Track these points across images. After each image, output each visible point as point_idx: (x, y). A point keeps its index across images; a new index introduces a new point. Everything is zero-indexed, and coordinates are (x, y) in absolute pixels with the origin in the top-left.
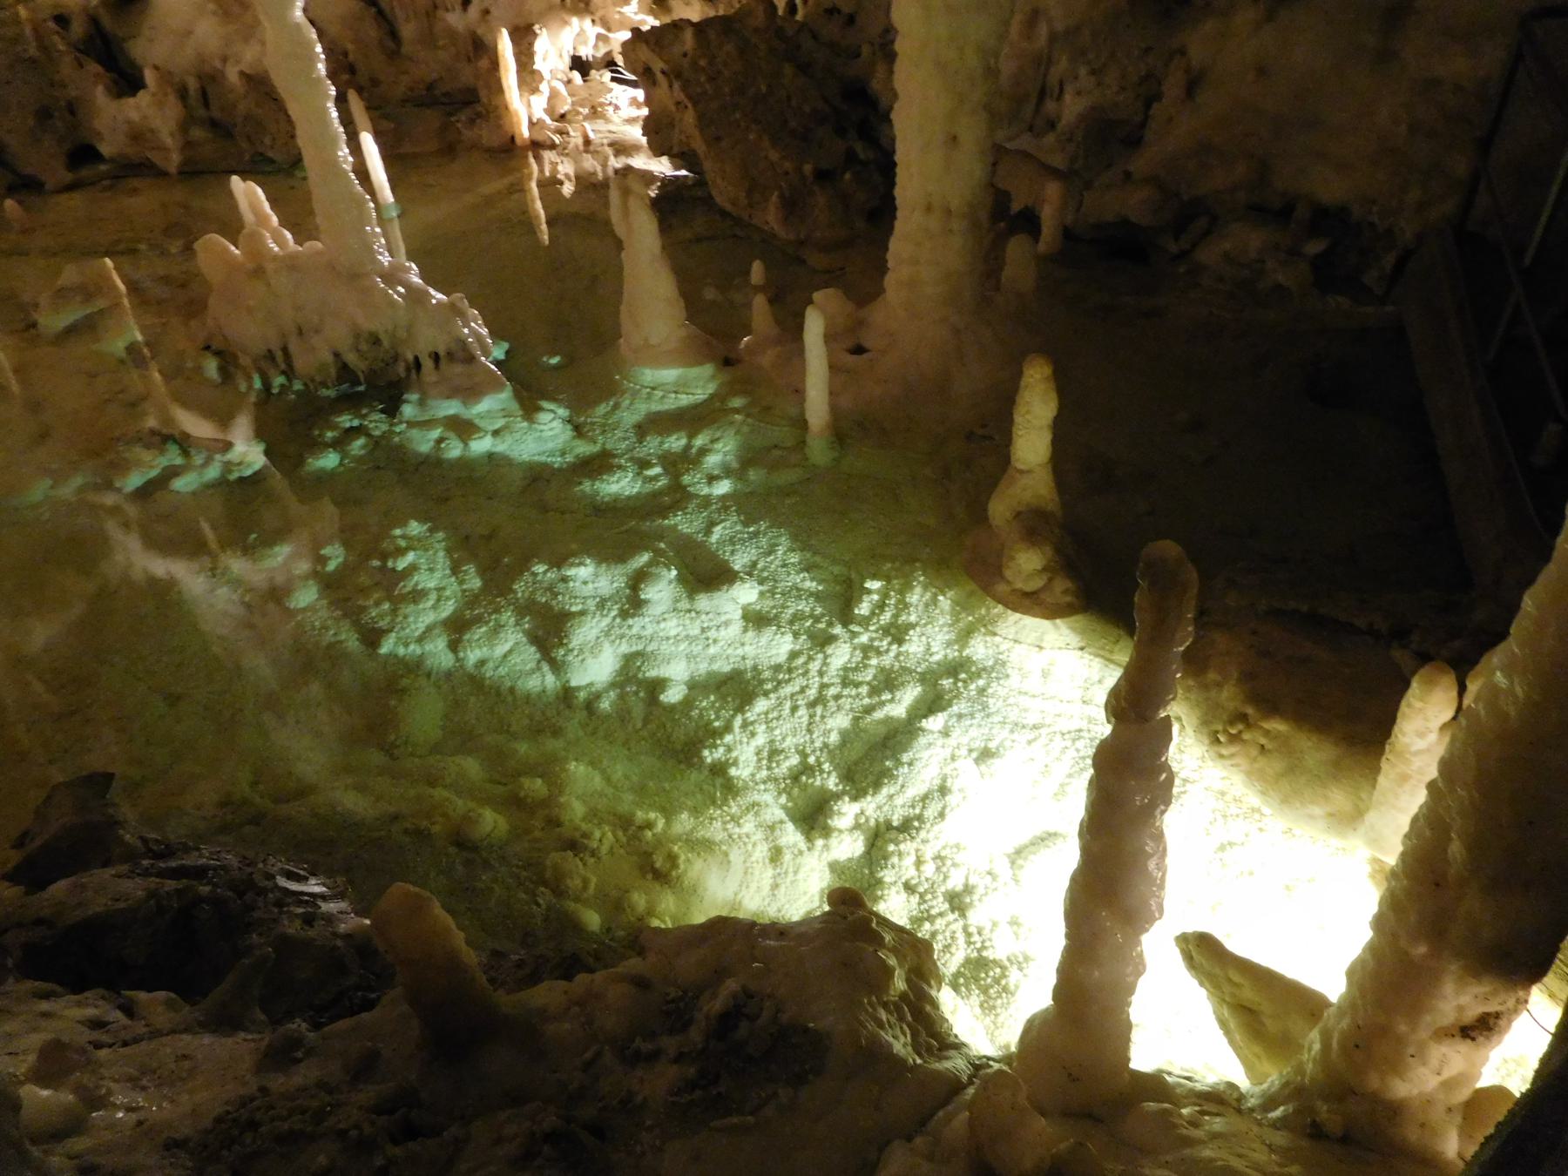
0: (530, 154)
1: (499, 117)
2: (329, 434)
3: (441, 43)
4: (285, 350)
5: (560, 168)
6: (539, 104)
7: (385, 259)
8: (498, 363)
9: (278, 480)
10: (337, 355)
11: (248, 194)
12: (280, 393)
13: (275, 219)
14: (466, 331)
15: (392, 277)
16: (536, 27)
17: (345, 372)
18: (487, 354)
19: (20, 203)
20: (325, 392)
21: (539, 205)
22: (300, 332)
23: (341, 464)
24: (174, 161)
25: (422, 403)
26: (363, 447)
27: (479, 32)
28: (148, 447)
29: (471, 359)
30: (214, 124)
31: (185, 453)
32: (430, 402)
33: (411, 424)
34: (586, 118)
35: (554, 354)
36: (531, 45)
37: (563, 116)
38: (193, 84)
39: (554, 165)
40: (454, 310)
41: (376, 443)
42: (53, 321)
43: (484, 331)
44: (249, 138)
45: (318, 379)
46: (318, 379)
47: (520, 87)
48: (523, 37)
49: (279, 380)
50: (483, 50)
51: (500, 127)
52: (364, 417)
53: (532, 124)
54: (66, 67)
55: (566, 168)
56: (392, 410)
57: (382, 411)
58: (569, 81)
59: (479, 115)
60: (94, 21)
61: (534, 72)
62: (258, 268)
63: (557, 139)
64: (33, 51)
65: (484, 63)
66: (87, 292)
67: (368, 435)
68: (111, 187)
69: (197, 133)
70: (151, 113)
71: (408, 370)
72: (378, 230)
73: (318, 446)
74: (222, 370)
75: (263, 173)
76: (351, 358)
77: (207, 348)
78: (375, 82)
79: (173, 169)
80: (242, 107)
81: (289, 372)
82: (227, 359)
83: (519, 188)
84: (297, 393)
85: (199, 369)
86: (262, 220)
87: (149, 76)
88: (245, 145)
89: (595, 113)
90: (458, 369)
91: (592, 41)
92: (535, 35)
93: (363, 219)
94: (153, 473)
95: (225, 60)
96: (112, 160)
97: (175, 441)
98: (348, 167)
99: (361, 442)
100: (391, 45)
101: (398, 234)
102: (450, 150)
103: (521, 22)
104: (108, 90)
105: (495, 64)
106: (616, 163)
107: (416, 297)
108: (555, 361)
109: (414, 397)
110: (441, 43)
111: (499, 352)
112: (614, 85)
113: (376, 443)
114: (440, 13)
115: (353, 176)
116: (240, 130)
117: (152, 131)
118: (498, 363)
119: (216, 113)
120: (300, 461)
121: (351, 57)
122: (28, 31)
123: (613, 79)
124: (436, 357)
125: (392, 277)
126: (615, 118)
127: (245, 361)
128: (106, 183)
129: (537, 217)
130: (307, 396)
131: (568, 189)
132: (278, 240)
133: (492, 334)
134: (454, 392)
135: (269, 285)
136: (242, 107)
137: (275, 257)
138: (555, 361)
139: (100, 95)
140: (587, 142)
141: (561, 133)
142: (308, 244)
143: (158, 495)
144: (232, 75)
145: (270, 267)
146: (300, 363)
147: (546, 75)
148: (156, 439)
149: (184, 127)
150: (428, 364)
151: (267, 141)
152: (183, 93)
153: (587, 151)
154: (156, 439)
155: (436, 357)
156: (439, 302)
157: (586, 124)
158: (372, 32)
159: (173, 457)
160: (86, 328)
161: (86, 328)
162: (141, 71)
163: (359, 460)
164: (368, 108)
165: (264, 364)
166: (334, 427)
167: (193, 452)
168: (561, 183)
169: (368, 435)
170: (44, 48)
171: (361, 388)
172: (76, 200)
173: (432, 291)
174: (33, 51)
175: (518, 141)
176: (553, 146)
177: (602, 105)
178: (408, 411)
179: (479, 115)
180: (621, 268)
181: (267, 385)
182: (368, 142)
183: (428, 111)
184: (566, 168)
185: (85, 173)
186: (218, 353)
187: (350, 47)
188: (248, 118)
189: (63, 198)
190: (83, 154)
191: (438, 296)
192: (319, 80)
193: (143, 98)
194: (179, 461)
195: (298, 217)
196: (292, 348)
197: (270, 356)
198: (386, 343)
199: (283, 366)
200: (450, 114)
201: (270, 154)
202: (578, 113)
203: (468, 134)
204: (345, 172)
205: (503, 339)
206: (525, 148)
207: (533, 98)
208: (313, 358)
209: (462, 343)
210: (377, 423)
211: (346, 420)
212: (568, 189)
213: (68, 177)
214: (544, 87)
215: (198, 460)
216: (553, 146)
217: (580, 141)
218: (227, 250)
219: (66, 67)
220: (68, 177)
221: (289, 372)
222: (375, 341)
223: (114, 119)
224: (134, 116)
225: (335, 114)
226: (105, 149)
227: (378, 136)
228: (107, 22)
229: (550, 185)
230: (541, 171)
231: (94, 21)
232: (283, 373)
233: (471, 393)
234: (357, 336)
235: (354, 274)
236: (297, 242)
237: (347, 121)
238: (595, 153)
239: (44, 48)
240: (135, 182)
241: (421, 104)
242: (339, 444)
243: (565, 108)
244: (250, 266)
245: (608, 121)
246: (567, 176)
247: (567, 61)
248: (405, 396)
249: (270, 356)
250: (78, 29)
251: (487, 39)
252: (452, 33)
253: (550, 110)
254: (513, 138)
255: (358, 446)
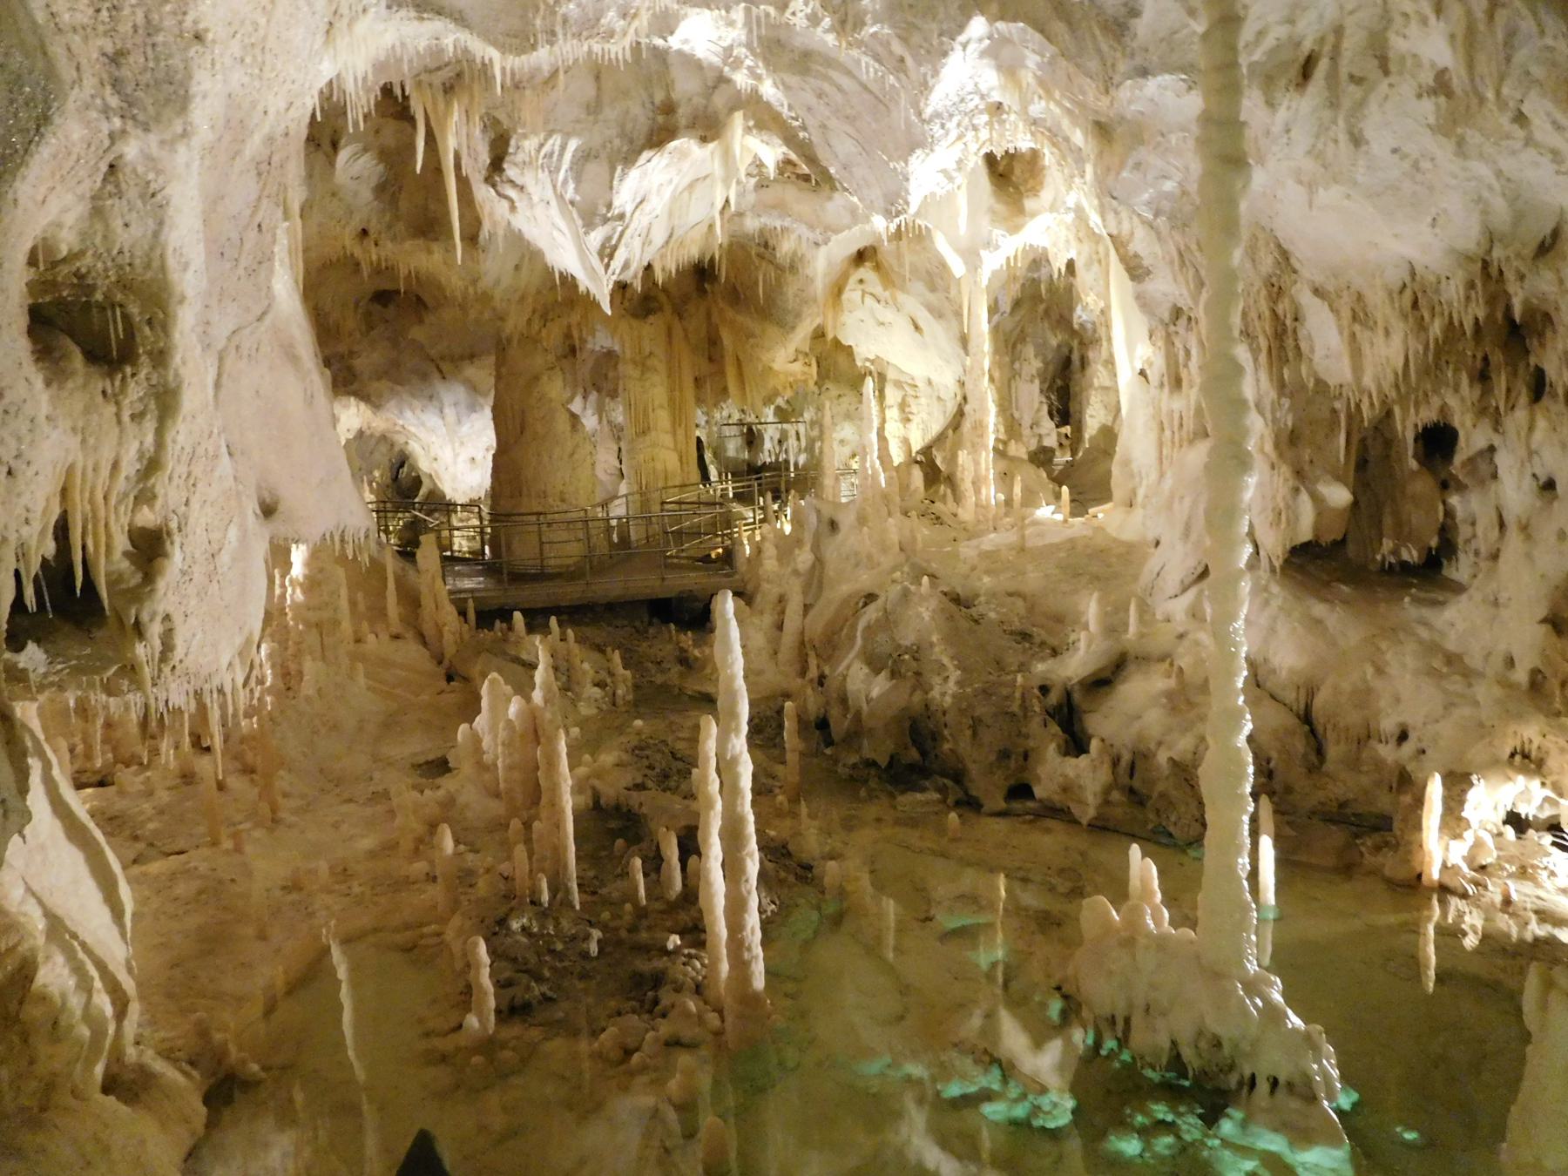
0: (1435, 897)
1: (1410, 852)
2: (1139, 1118)
3: (1365, 768)
4: (1127, 1021)
5: (1467, 918)
6: (1457, 852)
7: (1252, 967)
8: (1340, 1112)
9: (1074, 1146)
10: (1174, 1043)
11: (1142, 867)
12: (1108, 1057)
13: (1159, 896)
14: (1315, 1066)
15: (1252, 987)
16: (1474, 778)
17: (1176, 1062)
18: (1331, 1098)
19: (960, 816)
20: (1149, 1073)
21: (1431, 949)
22: (1147, 1009)
23: (1141, 1156)
24: (1088, 813)
25: (1244, 1125)
26: (1169, 1147)
27: (1409, 768)
28: (976, 1062)
29: (1312, 1099)
30: (1132, 791)
31: (1005, 1079)
32: (1254, 1129)
33: (1226, 1143)
34: (1510, 876)
35: (1410, 1128)
36: (1464, 792)
37: (1483, 868)
38: (1126, 757)
39: (1460, 915)
40: (1307, 1037)
41: (1184, 1148)
42: (949, 921)
43: (1335, 1073)
44: (1158, 811)
45: (1148, 1059)
46: (1148, 1059)
47: (1441, 829)
48: (1457, 783)
49: (1110, 1044)
50: (1407, 785)
51: (1407, 861)
52: (1179, 1115)
53: (1444, 866)
54: (1035, 725)
55: (1473, 920)
56: (1211, 1119)
57: (1200, 1117)
58: (1500, 834)
59: (1387, 844)
60: (1068, 694)
61: (1460, 819)
62: (1130, 939)
63: (1471, 889)
64: (1015, 708)
65: (1407, 799)
66: (972, 900)
67: (1178, 1137)
68: (1031, 822)
69: (1116, 796)
70: (1086, 776)
71: (1241, 1084)
72: (1254, 938)
73: (1122, 1125)
74: (1065, 1014)
75: (1159, 844)
76: (1187, 1053)
77: (1059, 988)
78: (1288, 790)
79: (1085, 822)
80: (1160, 787)
81: (1123, 1042)
82: (1072, 1009)
83: (1415, 929)
84: (1124, 1064)
85: (1044, 1006)
86: (1146, 893)
87: (1094, 745)
88: (1152, 816)
89: (1524, 873)
90: (1295, 1104)
91: (1537, 801)
92: (1472, 785)
93: (1242, 925)
94: (972, 1089)
95: (1160, 744)
96: (1041, 801)
97: (1000, 1065)
98: (1244, 875)
99: (1169, 1140)
100: (1313, 758)
101: (1269, 937)
102: (1347, 869)
103: (1459, 769)
104: (1059, 746)
105: (1419, 802)
106: (1536, 929)
107: (1272, 1015)
108: (1410, 1136)
109: (1238, 1114)
110: (1365, 768)
111: (1346, 1101)
112: (1555, 850)
113: (1184, 1148)
114: (1373, 743)
115: (1245, 883)
116: (1156, 808)
117: (1080, 787)
118: (1340, 1112)
119: (1136, 783)
120: (1102, 1135)
121: (1272, 765)
122: (1018, 695)
123: (1554, 844)
124: (1274, 1083)
125: (1252, 987)
126: (1548, 884)
127: (1085, 1013)
128: (1028, 817)
129: (1428, 959)
130: (1131, 1069)
131: (1470, 942)
132: (1156, 918)
133: (1344, 1078)
134: (1283, 1127)
135: (1134, 956)
136: (1160, 787)
137: (1149, 935)
138: (1410, 1136)
139: (1051, 750)
140: (1507, 901)
141: (1477, 884)
142: (1181, 930)
143: (965, 1112)
144: (1162, 757)
145: (1142, 941)
146: (1138, 1038)
147: (1474, 824)
148: (987, 1059)
149: (1107, 791)
150: (1263, 1087)
151: (1173, 819)
152: (1116, 762)
153: (1504, 911)
154: (987, 1059)
155: (1274, 1083)
156: (1295, 1030)
157: (1509, 882)
158: (1300, 745)
159: (992, 1080)
160: (965, 934)
161: (965, 934)
162: (1090, 738)
163: (1161, 1159)
164: (1276, 812)
165: (1104, 1027)
166: (1146, 1113)
167: (1012, 1084)
168: (1465, 934)
169: (1178, 1137)
170: (1024, 707)
171: (1187, 1083)
172: (999, 826)
173: (1290, 1012)
174: (1015, 708)
175: (1424, 878)
176: (1464, 896)
177: (1534, 867)
178: (1227, 1127)
179: (1387, 844)
180: (1522, 1060)
181: (1098, 1044)
182: (1267, 845)
183: (1334, 828)
184: (1473, 920)
185: (1017, 805)
186: (1066, 997)
187: (1274, 755)
188: (1162, 795)
189: (990, 820)
190: (1021, 791)
191: (1295, 1021)
192: (1242, 796)
193: (1083, 760)
194: (996, 1087)
195: (1179, 895)
196: (1135, 1022)
197: (1112, 1021)
198: (1226, 1050)
199: (1120, 1035)
200: (1357, 836)
201: (1171, 829)
202: (1503, 869)
203: (1370, 860)
204: (1240, 878)
205: (1355, 1087)
206: (1431, 889)
207: (1454, 844)
208: (1151, 1039)
209: (1308, 1080)
210: (1191, 1126)
211: (1161, 1111)
212: (1470, 942)
213: (1002, 805)
214: (1469, 836)
215: (1014, 1092)
216: (1464, 896)
217: (1498, 899)
218: (1109, 912)
219: (1035, 725)
220: (1002, 805)
221: (1123, 1042)
222: (1217, 1044)
223: (1055, 770)
224: (1071, 773)
225: (1246, 827)
226: (1038, 791)
227: (1278, 841)
228: (1077, 696)
229: (1450, 934)
230: (1444, 914)
231: (1068, 694)
232: (1118, 1039)
233: (1303, 1136)
234: (1200, 1033)
235: (1217, 975)
236: (1172, 923)
237: (1255, 834)
238: (1513, 915)
239: (1024, 707)
240: (1050, 823)
241: (1329, 819)
242: (1145, 1133)
243: (1488, 859)
244: (1124, 934)
245: (1538, 885)
246: (1473, 927)
247: (1502, 815)
248: (1229, 1110)
249: (1112, 1021)
250: (1054, 698)
251: (1417, 776)
252: (1379, 764)
253: (1470, 859)
254: (1419, 876)
255: (1164, 1142)
